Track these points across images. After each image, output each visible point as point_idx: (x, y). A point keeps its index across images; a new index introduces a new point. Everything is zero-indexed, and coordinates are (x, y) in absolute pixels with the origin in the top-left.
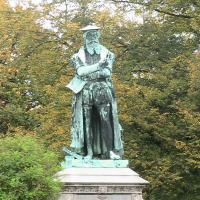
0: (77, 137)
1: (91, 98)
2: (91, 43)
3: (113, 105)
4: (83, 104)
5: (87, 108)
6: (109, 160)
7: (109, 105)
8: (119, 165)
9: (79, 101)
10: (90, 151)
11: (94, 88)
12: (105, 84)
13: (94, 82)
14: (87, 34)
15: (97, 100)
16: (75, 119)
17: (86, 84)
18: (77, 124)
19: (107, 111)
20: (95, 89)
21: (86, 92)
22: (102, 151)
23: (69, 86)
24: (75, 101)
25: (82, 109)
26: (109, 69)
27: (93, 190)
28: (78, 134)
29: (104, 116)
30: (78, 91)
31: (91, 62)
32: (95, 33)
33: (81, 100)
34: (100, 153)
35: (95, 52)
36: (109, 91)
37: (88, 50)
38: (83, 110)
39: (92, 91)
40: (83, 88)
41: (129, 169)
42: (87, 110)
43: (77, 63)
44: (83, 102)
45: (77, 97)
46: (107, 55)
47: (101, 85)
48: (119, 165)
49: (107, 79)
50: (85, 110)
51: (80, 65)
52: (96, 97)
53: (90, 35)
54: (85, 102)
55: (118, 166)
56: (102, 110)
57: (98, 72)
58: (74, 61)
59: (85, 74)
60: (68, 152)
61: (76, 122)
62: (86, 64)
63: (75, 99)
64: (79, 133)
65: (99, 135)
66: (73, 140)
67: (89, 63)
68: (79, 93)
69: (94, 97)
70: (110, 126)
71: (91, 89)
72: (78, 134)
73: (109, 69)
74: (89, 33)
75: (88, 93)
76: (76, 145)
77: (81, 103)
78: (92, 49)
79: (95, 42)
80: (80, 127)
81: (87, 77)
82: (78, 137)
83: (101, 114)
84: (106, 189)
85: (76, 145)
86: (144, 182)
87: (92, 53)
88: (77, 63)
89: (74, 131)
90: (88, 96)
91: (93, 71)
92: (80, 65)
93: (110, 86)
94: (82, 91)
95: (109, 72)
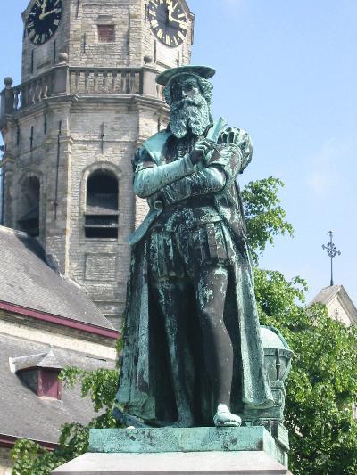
35: (189, 129)
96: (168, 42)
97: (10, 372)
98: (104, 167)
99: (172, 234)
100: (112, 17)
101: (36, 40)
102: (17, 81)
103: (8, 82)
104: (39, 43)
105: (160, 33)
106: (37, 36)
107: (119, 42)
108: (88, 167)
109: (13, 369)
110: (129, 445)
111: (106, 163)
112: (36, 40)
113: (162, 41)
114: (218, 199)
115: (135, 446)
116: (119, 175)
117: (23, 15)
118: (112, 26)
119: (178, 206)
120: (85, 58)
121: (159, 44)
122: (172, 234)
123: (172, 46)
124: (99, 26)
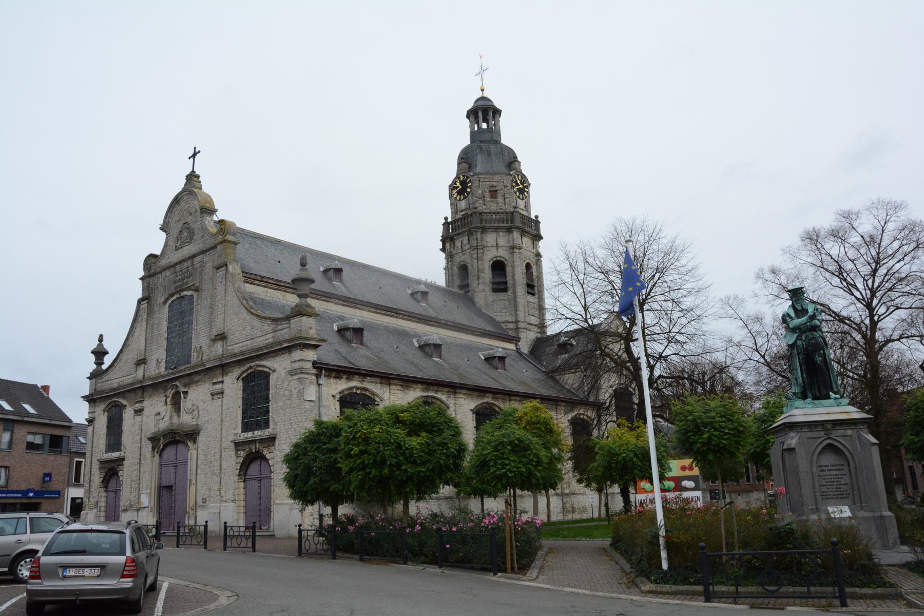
4: (798, 354)
7: (822, 352)
10: (809, 394)
11: (806, 338)
12: (816, 334)
21: (799, 343)
35: (802, 307)
37: (797, 306)
43: (788, 318)
44: (797, 351)
47: (813, 334)
53: (796, 294)
56: (817, 357)
62: (796, 319)
67: (798, 317)
68: (793, 344)
70: (826, 370)
72: (796, 380)
80: (797, 373)
88: (788, 318)
91: (803, 323)
94: (795, 342)
96: (521, 197)
97: (333, 329)
98: (499, 259)
99: (805, 341)
100: (496, 187)
101: (458, 199)
102: (450, 220)
103: (446, 219)
104: (460, 200)
105: (518, 194)
106: (459, 196)
107: (500, 199)
108: (492, 259)
109: (336, 329)
110: (808, 406)
111: (500, 257)
112: (458, 199)
113: (519, 197)
114: (817, 330)
115: (810, 406)
116: (506, 262)
117: (450, 186)
118: (496, 191)
119: (805, 332)
120: (484, 207)
121: (518, 199)
122: (805, 341)
123: (523, 199)
124: (490, 191)
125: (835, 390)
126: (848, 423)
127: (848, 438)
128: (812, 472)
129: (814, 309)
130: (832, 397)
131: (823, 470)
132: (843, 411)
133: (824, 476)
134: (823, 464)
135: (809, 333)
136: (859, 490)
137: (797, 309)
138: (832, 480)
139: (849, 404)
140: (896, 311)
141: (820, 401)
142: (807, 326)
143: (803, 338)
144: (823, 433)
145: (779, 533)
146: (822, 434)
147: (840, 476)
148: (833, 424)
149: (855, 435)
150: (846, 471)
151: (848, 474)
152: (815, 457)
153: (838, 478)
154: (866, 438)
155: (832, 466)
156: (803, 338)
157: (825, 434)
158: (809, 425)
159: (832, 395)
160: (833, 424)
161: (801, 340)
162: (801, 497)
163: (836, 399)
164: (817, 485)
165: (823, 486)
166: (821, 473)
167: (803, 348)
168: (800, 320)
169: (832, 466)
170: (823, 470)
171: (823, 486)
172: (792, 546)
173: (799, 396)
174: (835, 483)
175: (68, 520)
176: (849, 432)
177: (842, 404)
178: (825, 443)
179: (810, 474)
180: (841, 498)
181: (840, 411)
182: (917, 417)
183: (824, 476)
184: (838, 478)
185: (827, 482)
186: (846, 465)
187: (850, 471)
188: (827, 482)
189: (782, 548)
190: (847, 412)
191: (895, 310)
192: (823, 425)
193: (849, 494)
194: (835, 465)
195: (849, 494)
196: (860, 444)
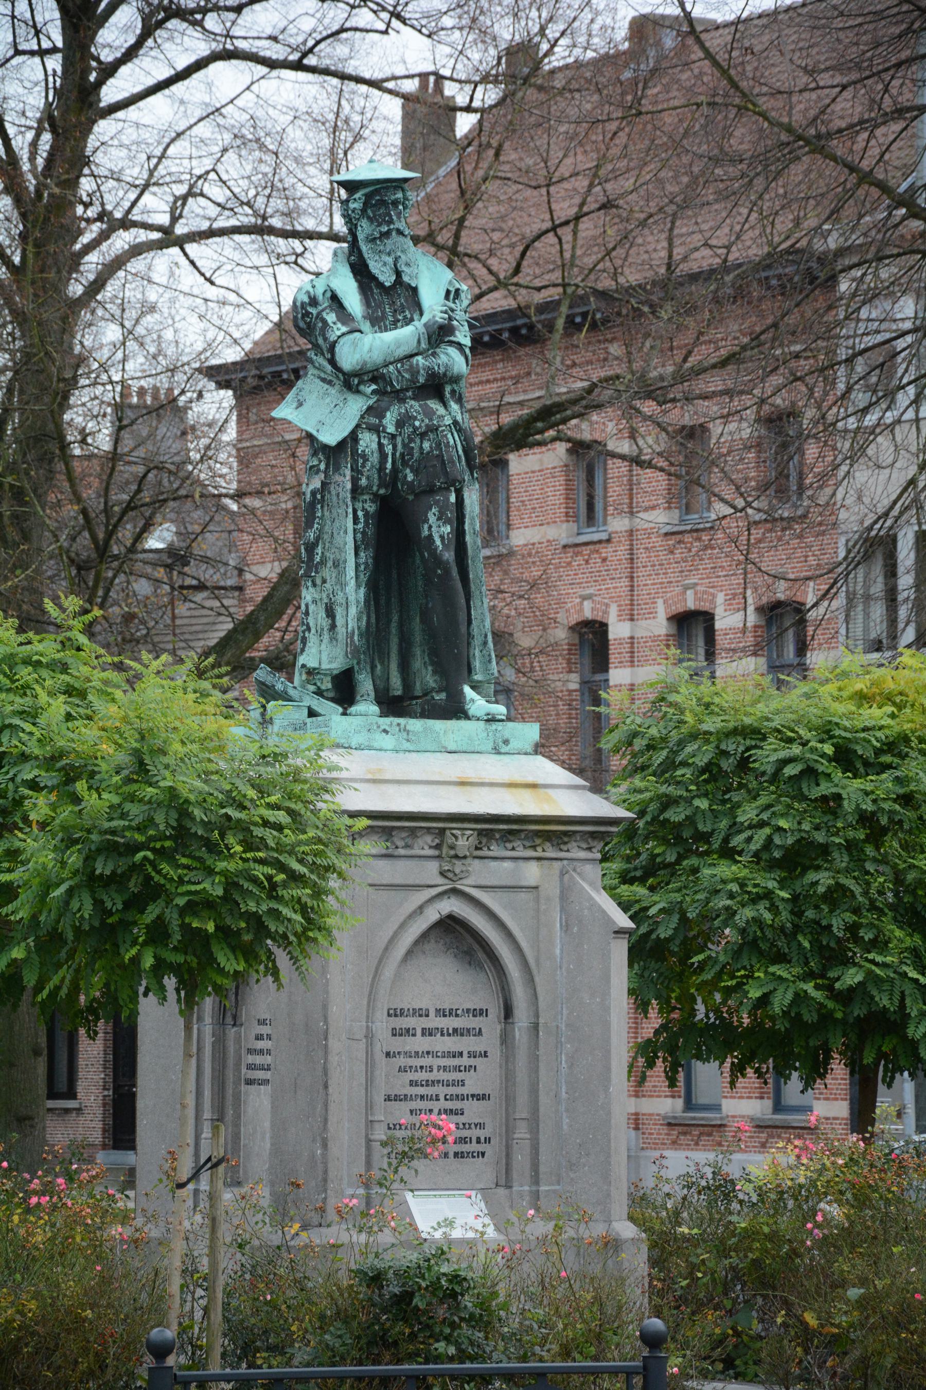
0: (325, 623)
1: (389, 465)
2: (387, 234)
3: (466, 495)
4: (356, 491)
5: (367, 506)
6: (463, 723)
7: (453, 498)
8: (506, 742)
9: (337, 478)
10: (365, 684)
11: (400, 424)
12: (441, 411)
13: (402, 401)
14: (368, 196)
15: (410, 477)
16: (319, 550)
17: (370, 408)
18: (328, 572)
19: (448, 521)
20: (408, 430)
21: (368, 442)
22: (407, 684)
23: (274, 414)
24: (322, 476)
25: (350, 510)
26: (460, 346)
27: (420, 842)
28: (330, 613)
29: (438, 542)
30: (340, 438)
31: (384, 317)
32: (399, 195)
33: (348, 473)
34: (399, 693)
35: (398, 274)
36: (453, 439)
37: (375, 267)
38: (355, 511)
39: (393, 437)
40: (358, 426)
41: (540, 757)
42: (366, 515)
43: (331, 317)
44: (355, 481)
45: (328, 459)
46: (448, 292)
47: (430, 413)
48: (506, 742)
49: (448, 389)
50: (360, 514)
51: (344, 329)
52: (405, 463)
53: (383, 203)
54: (363, 482)
55: (504, 749)
56: (432, 519)
57: (419, 358)
58: (314, 311)
59: (369, 367)
60: (279, 687)
61: (323, 562)
62: (366, 326)
63: (322, 466)
64: (339, 612)
65: (395, 618)
66: (312, 638)
67: (378, 322)
68: (342, 444)
69: (399, 463)
70: (459, 585)
71: (391, 429)
72: (330, 613)
73: (460, 346)
74: (376, 192)
75: (374, 446)
76: (324, 658)
77: (349, 486)
78: (390, 260)
79: (400, 232)
80: (343, 585)
81: (374, 380)
82: (333, 627)
83: (425, 532)
84: (473, 840)
85: (324, 658)
86: (613, 815)
87: (387, 278)
88: (331, 317)
89: (315, 602)
90: (375, 459)
91: (401, 352)
92: (344, 329)
93: (459, 418)
94: (353, 436)
95: (463, 360)
119: (399, 396)
125: (478, 677)
126: (538, 834)
127: (523, 896)
128: (369, 1036)
129: (447, 296)
130: (473, 710)
131: (409, 1032)
132: (518, 779)
133: (408, 1055)
134: (406, 1003)
135: (414, 406)
136: (534, 1121)
137: (374, 278)
138: (435, 1075)
139: (539, 749)
140: (218, 67)
141: (430, 722)
142: (414, 372)
143: (389, 422)
144: (433, 867)
145: (405, 1298)
146: (430, 871)
147: (465, 1061)
148: (481, 833)
149: (552, 889)
150: (490, 1040)
151: (495, 1053)
152: (389, 972)
153: (458, 1069)
154: (591, 898)
155: (441, 1013)
156: (389, 422)
157: (442, 874)
158: (388, 833)
159: (476, 703)
160: (481, 833)
161: (376, 430)
162: (325, 1146)
163: (491, 719)
164: (379, 1099)
165: (397, 1098)
166: (397, 1044)
167: (381, 468)
168: (389, 336)
169: (441, 1013)
170: (409, 1032)
171: (397, 1098)
172: (452, 1350)
173: (327, 685)
174: (441, 1091)
175: (553, 1223)
176: (532, 873)
177: (514, 745)
178: (432, 915)
179: (362, 1045)
180: (456, 1155)
181: (506, 779)
182: (668, 802)
183: (408, 1055)
184: (458, 1069)
185: (413, 1083)
186: (495, 1010)
187: (506, 1039)
188: (413, 1083)
189: (411, 1357)
190: (534, 786)
191: (215, 57)
192: (442, 831)
193: (488, 1140)
194: (453, 1013)
195: (488, 1140)
196: (566, 928)
